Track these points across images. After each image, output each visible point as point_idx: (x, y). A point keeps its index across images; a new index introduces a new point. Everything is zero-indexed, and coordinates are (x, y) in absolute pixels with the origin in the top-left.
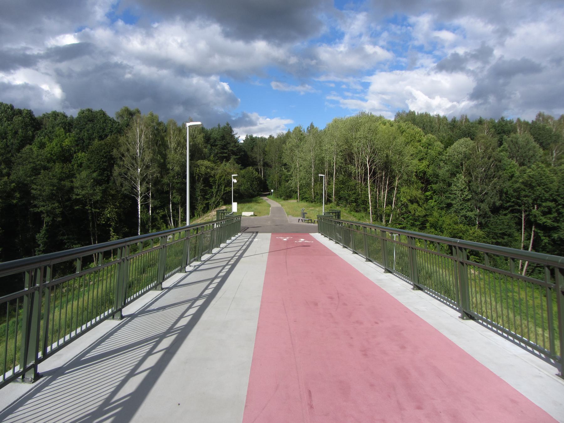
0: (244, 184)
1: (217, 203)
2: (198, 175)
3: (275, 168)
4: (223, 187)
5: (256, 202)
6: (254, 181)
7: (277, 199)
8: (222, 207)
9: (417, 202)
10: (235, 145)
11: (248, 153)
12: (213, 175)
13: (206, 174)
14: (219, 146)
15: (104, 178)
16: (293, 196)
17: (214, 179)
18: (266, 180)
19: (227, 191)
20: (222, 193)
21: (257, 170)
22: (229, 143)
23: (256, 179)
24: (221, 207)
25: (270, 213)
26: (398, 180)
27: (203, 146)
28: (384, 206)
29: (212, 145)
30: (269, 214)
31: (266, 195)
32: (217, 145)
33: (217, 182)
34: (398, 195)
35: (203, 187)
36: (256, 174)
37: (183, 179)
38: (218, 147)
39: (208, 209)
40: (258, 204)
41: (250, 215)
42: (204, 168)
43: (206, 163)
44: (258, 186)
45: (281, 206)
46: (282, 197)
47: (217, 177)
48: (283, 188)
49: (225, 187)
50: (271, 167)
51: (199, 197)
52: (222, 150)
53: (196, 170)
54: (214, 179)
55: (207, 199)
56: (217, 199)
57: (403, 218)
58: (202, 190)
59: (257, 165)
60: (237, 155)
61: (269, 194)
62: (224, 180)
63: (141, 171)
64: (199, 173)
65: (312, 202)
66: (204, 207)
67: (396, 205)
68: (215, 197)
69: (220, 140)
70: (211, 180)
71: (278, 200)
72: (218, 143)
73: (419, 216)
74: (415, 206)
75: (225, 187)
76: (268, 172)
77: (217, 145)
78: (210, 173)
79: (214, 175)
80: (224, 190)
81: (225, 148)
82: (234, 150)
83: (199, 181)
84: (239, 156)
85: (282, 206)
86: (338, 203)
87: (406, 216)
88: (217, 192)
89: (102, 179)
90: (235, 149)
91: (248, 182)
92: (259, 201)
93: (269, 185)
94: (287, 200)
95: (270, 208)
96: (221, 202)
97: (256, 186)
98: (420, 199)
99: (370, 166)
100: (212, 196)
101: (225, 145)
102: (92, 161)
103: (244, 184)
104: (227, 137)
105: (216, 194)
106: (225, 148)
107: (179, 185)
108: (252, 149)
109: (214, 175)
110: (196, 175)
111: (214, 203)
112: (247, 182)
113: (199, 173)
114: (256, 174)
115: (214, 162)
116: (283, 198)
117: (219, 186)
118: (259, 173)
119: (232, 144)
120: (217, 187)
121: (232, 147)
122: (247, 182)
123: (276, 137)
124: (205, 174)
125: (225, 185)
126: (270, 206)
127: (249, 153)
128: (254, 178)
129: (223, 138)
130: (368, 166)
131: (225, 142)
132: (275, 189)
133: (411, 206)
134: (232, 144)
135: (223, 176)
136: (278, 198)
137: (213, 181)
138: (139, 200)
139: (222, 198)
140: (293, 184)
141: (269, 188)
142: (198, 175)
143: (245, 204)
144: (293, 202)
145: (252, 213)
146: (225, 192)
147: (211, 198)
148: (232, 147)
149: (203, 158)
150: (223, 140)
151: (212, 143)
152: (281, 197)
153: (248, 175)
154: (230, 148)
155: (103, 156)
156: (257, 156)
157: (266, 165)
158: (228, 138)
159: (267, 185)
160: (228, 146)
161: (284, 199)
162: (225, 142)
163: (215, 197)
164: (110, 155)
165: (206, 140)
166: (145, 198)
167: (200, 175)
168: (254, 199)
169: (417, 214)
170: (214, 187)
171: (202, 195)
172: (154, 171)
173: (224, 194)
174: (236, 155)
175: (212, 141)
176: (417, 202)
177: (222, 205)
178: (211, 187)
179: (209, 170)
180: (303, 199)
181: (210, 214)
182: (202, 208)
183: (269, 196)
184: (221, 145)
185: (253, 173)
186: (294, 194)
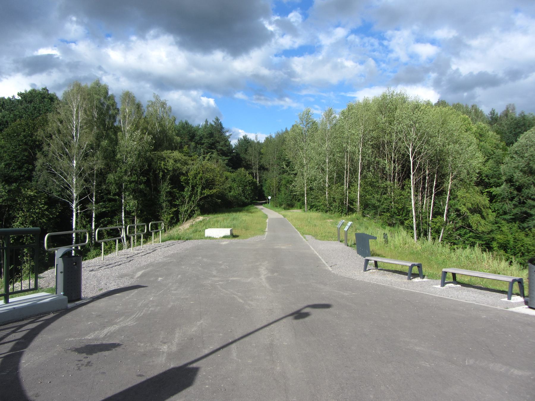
0: (234, 189)
1: (191, 212)
2: (163, 171)
3: (273, 172)
4: (199, 190)
5: (248, 211)
6: (247, 186)
7: (275, 208)
8: (198, 217)
9: (480, 212)
10: (225, 144)
11: (241, 155)
12: (184, 172)
13: (174, 170)
14: (205, 144)
15: (23, 173)
16: (295, 205)
17: (186, 178)
18: (262, 186)
19: (205, 195)
20: (199, 197)
21: (252, 174)
22: (218, 142)
23: (250, 184)
24: (196, 218)
25: (267, 230)
26: (452, 180)
27: (174, 133)
28: (429, 217)
29: (197, 143)
30: (263, 231)
31: (261, 204)
32: (203, 144)
33: (191, 181)
34: (452, 202)
35: (170, 188)
36: (249, 177)
37: (140, 176)
38: (204, 146)
39: (178, 221)
40: (250, 214)
41: (222, 235)
42: (171, 161)
43: (176, 154)
44: (251, 193)
45: (282, 217)
46: (282, 205)
47: (191, 174)
48: (283, 195)
49: (203, 188)
50: (267, 169)
51: (164, 202)
52: (209, 150)
53: (160, 163)
54: (186, 178)
55: (175, 206)
56: (191, 206)
57: (460, 235)
58: (170, 194)
59: (251, 168)
60: (228, 156)
61: (266, 203)
62: (201, 178)
63: (77, 163)
64: (164, 168)
65: (326, 212)
66: (172, 218)
67: (447, 216)
68: (188, 203)
69: (207, 138)
70: (183, 178)
71: (277, 210)
72: (205, 141)
73: (483, 232)
74: (476, 217)
75: (203, 188)
76: (264, 176)
77: (203, 144)
78: (181, 169)
79: (187, 172)
80: (201, 194)
81: (213, 147)
82: (225, 150)
83: (165, 181)
84: (230, 157)
85: (284, 217)
86: (363, 212)
87: (463, 232)
88: (190, 197)
89: (21, 176)
90: (225, 149)
91: (240, 186)
92: (252, 210)
93: (266, 191)
94: (289, 209)
95: (267, 221)
96: (197, 210)
97: (249, 192)
98: (484, 208)
99: (414, 158)
100: (183, 203)
101: (213, 144)
102: (5, 149)
103: (234, 189)
104: (216, 134)
105: (190, 200)
106: (213, 147)
107: (133, 185)
108: (246, 150)
109: (187, 172)
110: (160, 172)
111: (186, 211)
112: (239, 186)
113: (164, 168)
114: (249, 177)
115: (187, 154)
116: (283, 206)
117: (193, 188)
118: (254, 178)
119: (222, 143)
120: (190, 189)
121: (222, 146)
122: (239, 186)
123: (274, 136)
124: (174, 169)
125: (202, 187)
126: (266, 217)
127: (242, 156)
128: (246, 182)
129: (211, 135)
130: (411, 159)
131: (213, 140)
132: (273, 196)
133: (472, 218)
134: (222, 143)
135: (199, 173)
136: (276, 206)
137: (185, 179)
138: (74, 206)
139: (198, 205)
140: (298, 188)
141: (266, 195)
142: (163, 171)
143: (231, 214)
144: (296, 213)
145: (227, 232)
146: (203, 196)
147: (182, 205)
148: (222, 146)
149: (173, 149)
150: (210, 138)
151: (198, 141)
152: (281, 205)
153: (239, 178)
154: (219, 147)
155: (22, 140)
156: (252, 158)
157: (262, 168)
158: (216, 135)
159: (264, 191)
160: (217, 144)
161: (285, 209)
162: (213, 140)
163: (188, 203)
164: (32, 141)
165: (190, 137)
166: (84, 203)
167: (166, 171)
168: (246, 208)
169: (481, 229)
170: (186, 189)
171: (168, 201)
172: (97, 163)
173: (201, 199)
174: (226, 156)
175: (197, 138)
176: (480, 212)
177: (199, 215)
178: (182, 189)
179: (179, 165)
180: (312, 207)
181: (180, 227)
182: (169, 219)
183: (266, 205)
184: (208, 143)
185: (245, 176)
186: (296, 202)
